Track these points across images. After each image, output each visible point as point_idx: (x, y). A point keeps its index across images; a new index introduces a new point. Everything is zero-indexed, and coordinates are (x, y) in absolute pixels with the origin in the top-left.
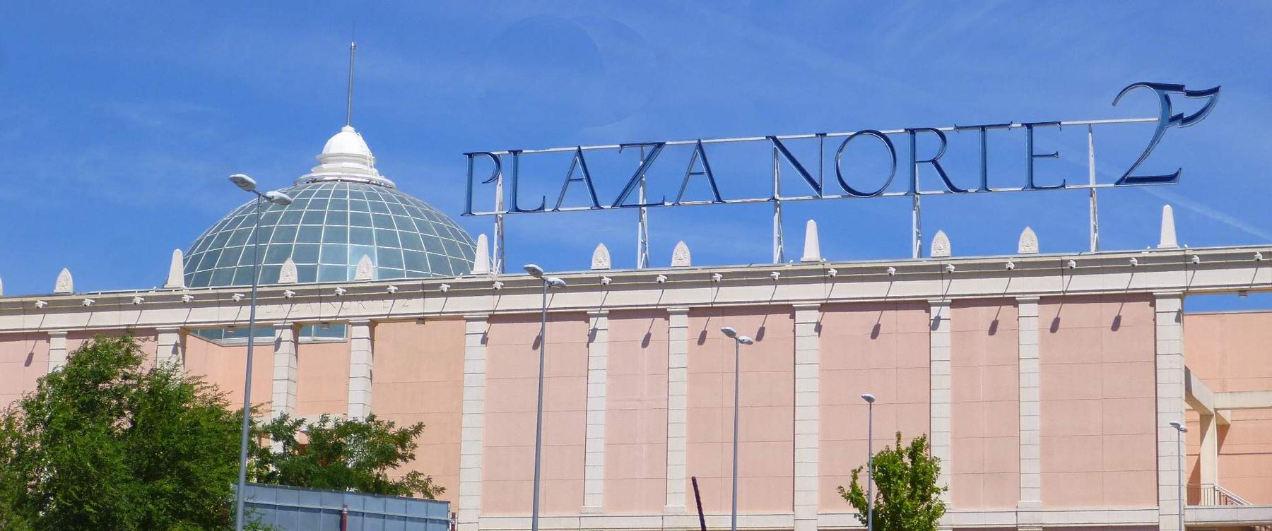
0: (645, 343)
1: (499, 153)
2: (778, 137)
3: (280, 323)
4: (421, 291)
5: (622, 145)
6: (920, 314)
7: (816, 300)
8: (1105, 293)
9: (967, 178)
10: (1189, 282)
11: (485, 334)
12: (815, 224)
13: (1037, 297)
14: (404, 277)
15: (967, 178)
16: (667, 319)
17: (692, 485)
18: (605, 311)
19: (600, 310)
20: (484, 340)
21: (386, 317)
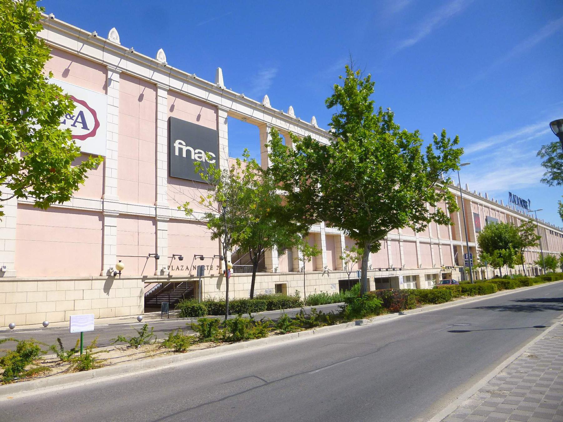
13: (168, 88)
19: (116, 69)
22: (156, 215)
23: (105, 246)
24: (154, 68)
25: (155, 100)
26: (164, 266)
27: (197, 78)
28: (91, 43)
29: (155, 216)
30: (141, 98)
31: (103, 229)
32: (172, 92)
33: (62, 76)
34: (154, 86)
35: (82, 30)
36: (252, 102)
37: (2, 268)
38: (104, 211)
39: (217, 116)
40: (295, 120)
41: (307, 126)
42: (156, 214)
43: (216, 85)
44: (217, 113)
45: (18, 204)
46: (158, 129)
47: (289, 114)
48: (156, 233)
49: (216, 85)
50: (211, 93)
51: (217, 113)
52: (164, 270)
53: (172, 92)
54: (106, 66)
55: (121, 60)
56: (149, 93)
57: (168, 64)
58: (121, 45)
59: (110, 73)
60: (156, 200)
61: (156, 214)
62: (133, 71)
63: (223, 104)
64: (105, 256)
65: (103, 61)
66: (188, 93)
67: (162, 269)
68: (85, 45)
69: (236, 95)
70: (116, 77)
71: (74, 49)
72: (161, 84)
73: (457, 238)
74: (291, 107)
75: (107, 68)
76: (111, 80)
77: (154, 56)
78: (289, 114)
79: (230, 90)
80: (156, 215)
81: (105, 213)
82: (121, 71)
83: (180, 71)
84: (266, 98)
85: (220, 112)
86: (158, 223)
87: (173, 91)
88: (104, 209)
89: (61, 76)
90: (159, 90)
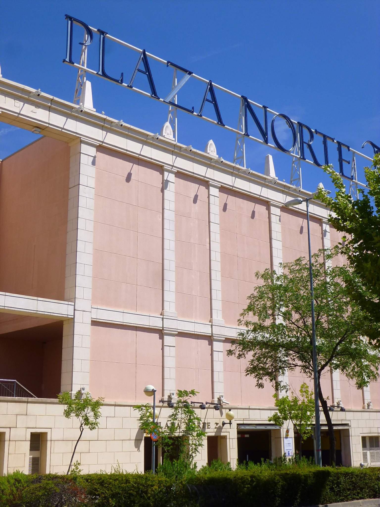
0: (195, 201)
1: (294, 121)
2: (350, 148)
3: (169, 168)
4: (49, 104)
5: (168, 62)
6: (156, 174)
7: (280, 202)
8: (300, 210)
9: (321, 159)
10: (103, 140)
11: (95, 157)
12: (90, 83)
13: (219, 185)
14: (298, 185)
15: (321, 159)
16: (208, 188)
17: (199, 341)
18: (175, 170)
19: (172, 168)
20: (94, 163)
21: (17, 115)
22: (212, 334)
23: (165, 369)
24: (236, 174)
25: (34, 144)
26: (221, 394)
27: (194, 150)
28: (246, 178)
29: (211, 335)
30: (128, 178)
31: (212, 355)
32: (224, 189)
33: (223, 211)
34: (267, 203)
35: (132, 127)
36: (129, 128)
37: (81, 390)
38: (164, 329)
39: (269, 214)
40: (216, 162)
41: (180, 151)
42: (163, 326)
43: (77, 106)
44: (268, 209)
45: (92, 321)
46: (211, 233)
47: (206, 152)
48: (163, 349)
49: (77, 106)
50: (146, 145)
51: (268, 209)
52: (172, 396)
53: (224, 189)
54: (208, 182)
55: (207, 169)
56: (261, 209)
57: (279, 180)
58: (97, 111)
59: (166, 174)
60: (163, 309)
61: (163, 326)
62: (255, 193)
63: (195, 172)
64: (165, 380)
65: (49, 124)
66: (127, 150)
67: (219, 397)
68: (26, 104)
69: (148, 135)
70: (171, 177)
71: (98, 139)
72: (213, 181)
73: (67, 296)
74: (211, 142)
75: (163, 168)
76: (167, 181)
77: (205, 150)
78: (206, 152)
79: (101, 113)
80: (212, 334)
81: (165, 331)
82: (98, 144)
83: (132, 127)
84: (167, 127)
85: (272, 208)
86: (214, 343)
87: (111, 150)
88: (164, 327)
89: (125, 181)
90: (211, 188)
